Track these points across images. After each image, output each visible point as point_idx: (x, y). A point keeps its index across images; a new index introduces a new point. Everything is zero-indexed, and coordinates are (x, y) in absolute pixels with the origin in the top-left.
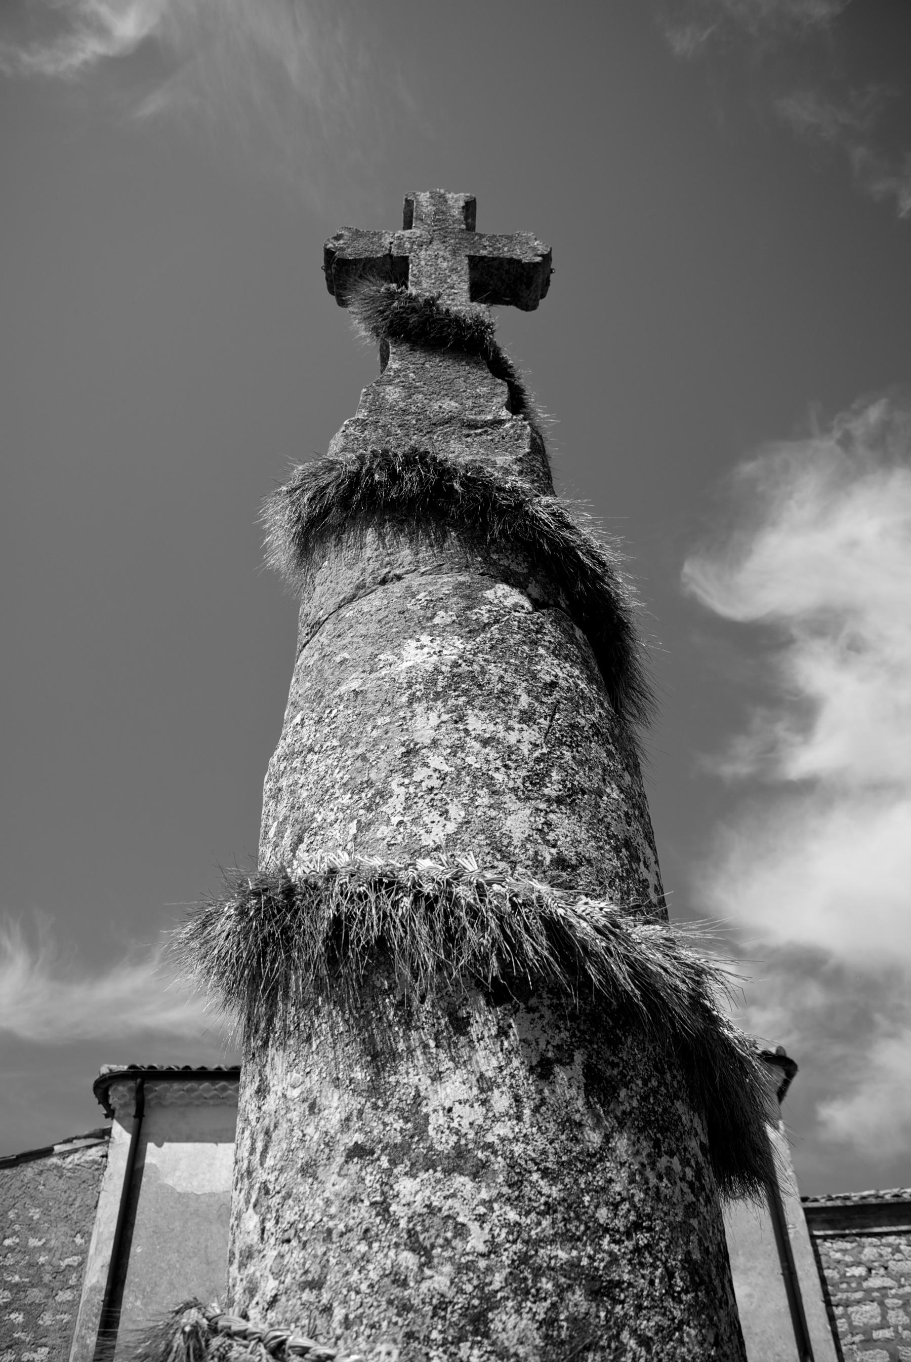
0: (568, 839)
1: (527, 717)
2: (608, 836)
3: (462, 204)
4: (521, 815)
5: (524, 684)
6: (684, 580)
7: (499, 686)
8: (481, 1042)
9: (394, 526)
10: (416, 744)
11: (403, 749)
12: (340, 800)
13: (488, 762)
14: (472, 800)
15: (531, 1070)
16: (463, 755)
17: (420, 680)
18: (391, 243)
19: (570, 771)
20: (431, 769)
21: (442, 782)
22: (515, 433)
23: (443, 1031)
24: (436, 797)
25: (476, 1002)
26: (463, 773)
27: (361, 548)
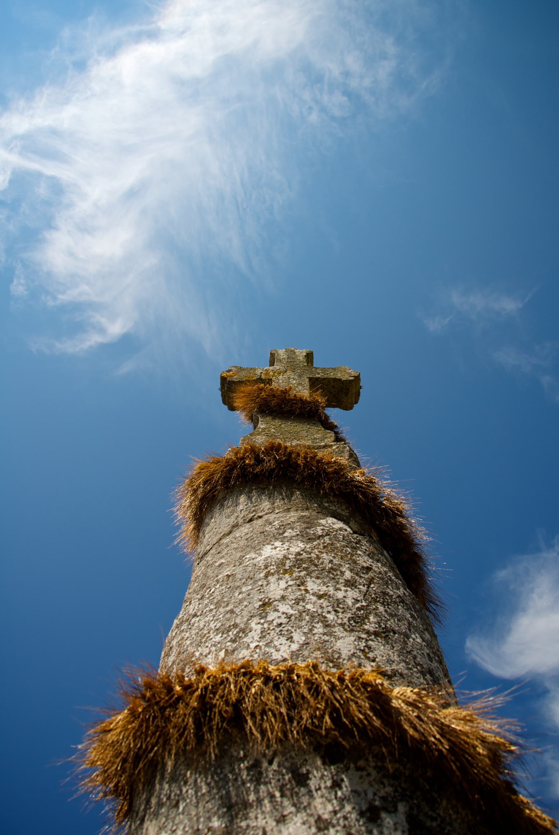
0: (384, 658)
1: (350, 584)
2: (415, 663)
3: (305, 354)
4: (347, 640)
5: (347, 566)
6: (467, 652)
7: (330, 565)
8: (319, 792)
9: (259, 492)
10: (270, 599)
11: (261, 603)
12: (214, 639)
13: (322, 607)
14: (311, 630)
15: (362, 814)
16: (304, 604)
17: (273, 563)
18: (261, 373)
19: (383, 618)
20: (280, 613)
21: (288, 620)
22: (339, 450)
23: (286, 785)
24: (284, 629)
25: (314, 762)
26: (304, 614)
27: (236, 506)
